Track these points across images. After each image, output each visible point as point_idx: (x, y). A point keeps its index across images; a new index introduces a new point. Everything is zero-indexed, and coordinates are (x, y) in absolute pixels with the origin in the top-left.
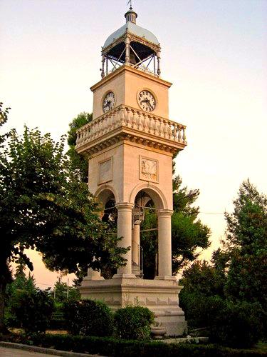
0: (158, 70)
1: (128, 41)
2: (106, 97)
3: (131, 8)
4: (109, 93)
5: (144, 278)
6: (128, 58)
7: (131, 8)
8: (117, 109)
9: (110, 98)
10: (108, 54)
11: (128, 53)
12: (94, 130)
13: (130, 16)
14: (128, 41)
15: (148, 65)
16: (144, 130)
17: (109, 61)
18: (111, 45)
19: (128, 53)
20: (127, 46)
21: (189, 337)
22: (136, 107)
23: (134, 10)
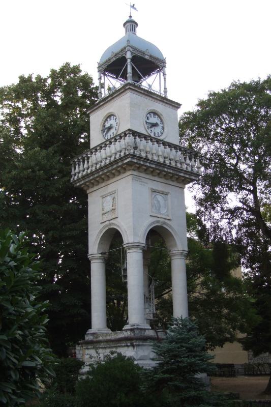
0: (165, 88)
1: (129, 56)
2: (106, 120)
3: (130, 17)
4: (110, 116)
5: (233, 364)
6: (129, 75)
7: (130, 17)
8: (123, 135)
9: (112, 122)
10: (106, 70)
11: (129, 70)
12: (94, 158)
13: (131, 25)
14: (129, 56)
15: (152, 82)
16: (176, 165)
17: (105, 77)
18: (109, 60)
19: (129, 70)
20: (129, 61)
21: (56, 279)
22: (177, 143)
23: (133, 18)
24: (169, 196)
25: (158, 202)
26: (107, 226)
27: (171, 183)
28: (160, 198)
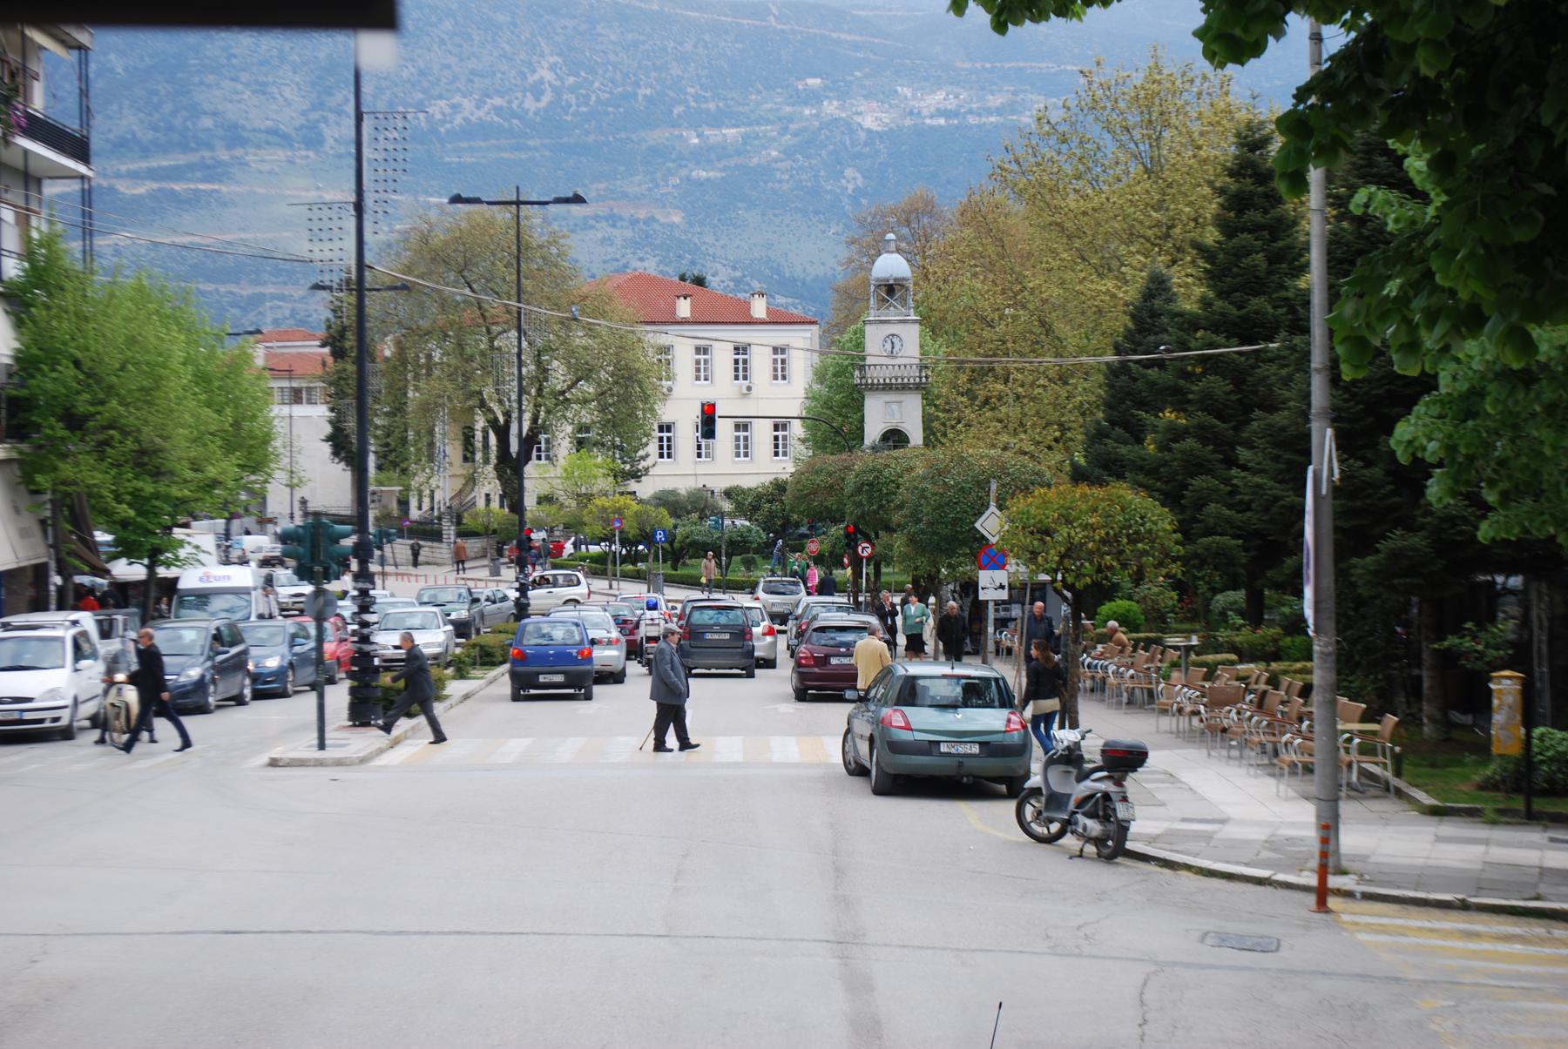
28: (894, 406)
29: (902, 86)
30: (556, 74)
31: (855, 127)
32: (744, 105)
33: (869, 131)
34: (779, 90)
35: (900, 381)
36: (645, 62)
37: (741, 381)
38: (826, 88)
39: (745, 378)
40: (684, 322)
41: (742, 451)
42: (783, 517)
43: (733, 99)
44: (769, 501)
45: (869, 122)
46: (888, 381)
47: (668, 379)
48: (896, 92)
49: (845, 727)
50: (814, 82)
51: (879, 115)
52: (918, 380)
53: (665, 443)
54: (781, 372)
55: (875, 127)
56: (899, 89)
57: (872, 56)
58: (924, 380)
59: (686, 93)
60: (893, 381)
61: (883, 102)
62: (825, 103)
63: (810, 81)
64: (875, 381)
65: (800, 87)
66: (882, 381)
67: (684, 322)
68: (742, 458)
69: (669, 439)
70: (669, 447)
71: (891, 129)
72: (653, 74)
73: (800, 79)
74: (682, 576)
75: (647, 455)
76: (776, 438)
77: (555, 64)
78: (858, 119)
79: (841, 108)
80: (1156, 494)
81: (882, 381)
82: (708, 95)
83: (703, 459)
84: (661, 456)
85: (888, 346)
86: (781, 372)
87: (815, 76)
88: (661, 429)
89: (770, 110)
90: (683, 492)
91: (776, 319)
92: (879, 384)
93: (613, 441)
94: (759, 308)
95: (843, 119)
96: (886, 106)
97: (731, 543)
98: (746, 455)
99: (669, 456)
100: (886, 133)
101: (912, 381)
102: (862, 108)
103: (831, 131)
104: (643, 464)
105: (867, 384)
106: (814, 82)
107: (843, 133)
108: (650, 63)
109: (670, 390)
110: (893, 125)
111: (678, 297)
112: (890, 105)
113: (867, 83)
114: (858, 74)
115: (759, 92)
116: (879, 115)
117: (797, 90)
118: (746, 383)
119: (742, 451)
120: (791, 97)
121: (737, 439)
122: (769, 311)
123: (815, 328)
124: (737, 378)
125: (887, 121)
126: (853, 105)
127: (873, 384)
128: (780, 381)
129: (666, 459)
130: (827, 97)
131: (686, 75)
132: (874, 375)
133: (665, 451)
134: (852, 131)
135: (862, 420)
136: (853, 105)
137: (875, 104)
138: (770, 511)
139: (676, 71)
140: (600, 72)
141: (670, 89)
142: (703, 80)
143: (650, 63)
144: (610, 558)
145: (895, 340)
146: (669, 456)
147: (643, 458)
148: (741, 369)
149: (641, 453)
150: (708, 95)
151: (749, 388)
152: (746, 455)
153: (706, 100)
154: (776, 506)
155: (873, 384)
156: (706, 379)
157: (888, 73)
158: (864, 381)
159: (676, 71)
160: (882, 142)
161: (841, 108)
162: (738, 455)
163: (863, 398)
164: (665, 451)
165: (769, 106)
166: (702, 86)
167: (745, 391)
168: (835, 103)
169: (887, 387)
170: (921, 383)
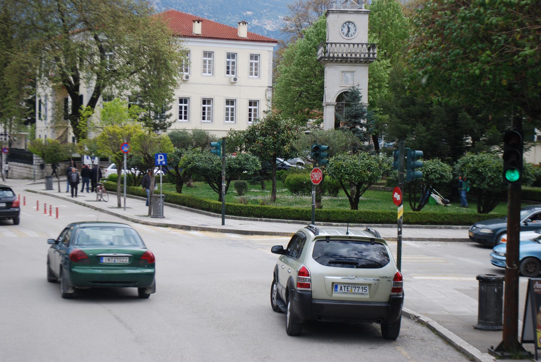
24: (355, 72)
25: (347, 78)
26: (346, 89)
27: (357, 65)
28: (348, 75)
29: (280, 15)
30: (159, 7)
31: (263, 29)
32: (224, 20)
33: (268, 31)
34: (237, 15)
35: (353, 56)
36: (190, 3)
37: (230, 75)
38: (254, 15)
39: (233, 73)
40: (197, 36)
41: (230, 117)
42: (275, 149)
43: (221, 18)
44: (262, 135)
45: (268, 28)
46: (345, 55)
47: (187, 71)
48: (278, 18)
49: (272, 279)
50: (249, 13)
51: (272, 25)
52: (367, 56)
53: (183, 110)
54: (254, 70)
55: (270, 29)
56: (279, 17)
57: (270, 5)
58: (371, 56)
59: (204, 15)
60: (349, 56)
61: (273, 21)
62: (253, 20)
63: (248, 13)
64: (336, 55)
65: (244, 14)
66: (340, 55)
67: (197, 36)
68: (230, 121)
69: (186, 108)
70: (185, 113)
71: (276, 30)
72: (193, 8)
73: (244, 12)
74: (184, 198)
75: (171, 115)
76: (250, 110)
77: (158, 3)
78: (264, 26)
79: (259, 22)
80: (446, 162)
81: (340, 55)
82: (212, 16)
83: (206, 121)
84: (181, 118)
85: (345, 30)
86: (254, 70)
87: (250, 11)
88: (181, 101)
89: (234, 22)
90: (190, 132)
91: (253, 39)
92: (338, 58)
93: (149, 105)
94: (243, 32)
95: (259, 26)
96: (274, 22)
97: (230, 170)
98: (232, 119)
99: (185, 118)
100: (274, 32)
101: (362, 56)
102: (266, 23)
103: (255, 30)
104: (168, 120)
105: (329, 57)
106: (249, 13)
107: (259, 31)
108: (192, 4)
109: (187, 77)
110: (277, 29)
111: (194, 21)
112: (276, 22)
113: (268, 14)
114: (265, 11)
115: (230, 16)
116: (272, 25)
117: (243, 16)
118: (234, 76)
119: (230, 117)
120: (241, 18)
121: (227, 109)
122: (248, 34)
123: (275, 45)
124: (228, 73)
125: (274, 27)
126: (263, 22)
127: (333, 57)
128: (254, 76)
129: (183, 120)
130: (254, 18)
131: (204, 9)
132: (336, 51)
133: (183, 115)
134: (262, 31)
135: (322, 87)
136: (263, 22)
137: (270, 22)
138: (264, 144)
139: (201, 7)
140: (174, 6)
141: (199, 13)
142: (210, 11)
143: (192, 4)
144: (120, 179)
145: (351, 26)
146: (185, 118)
147: (168, 117)
148: (230, 69)
149: (167, 113)
150: (212, 16)
151: (235, 79)
152: (232, 119)
153: (211, 18)
154: (269, 139)
155: (333, 57)
156: (209, 73)
157: (275, 11)
158: (327, 55)
159: (201, 7)
160: (272, 35)
161: (259, 22)
162: (227, 119)
163: (322, 72)
164: (183, 115)
165: (233, 21)
166: (210, 13)
167: (233, 81)
168: (257, 20)
169: (344, 60)
170: (369, 58)
